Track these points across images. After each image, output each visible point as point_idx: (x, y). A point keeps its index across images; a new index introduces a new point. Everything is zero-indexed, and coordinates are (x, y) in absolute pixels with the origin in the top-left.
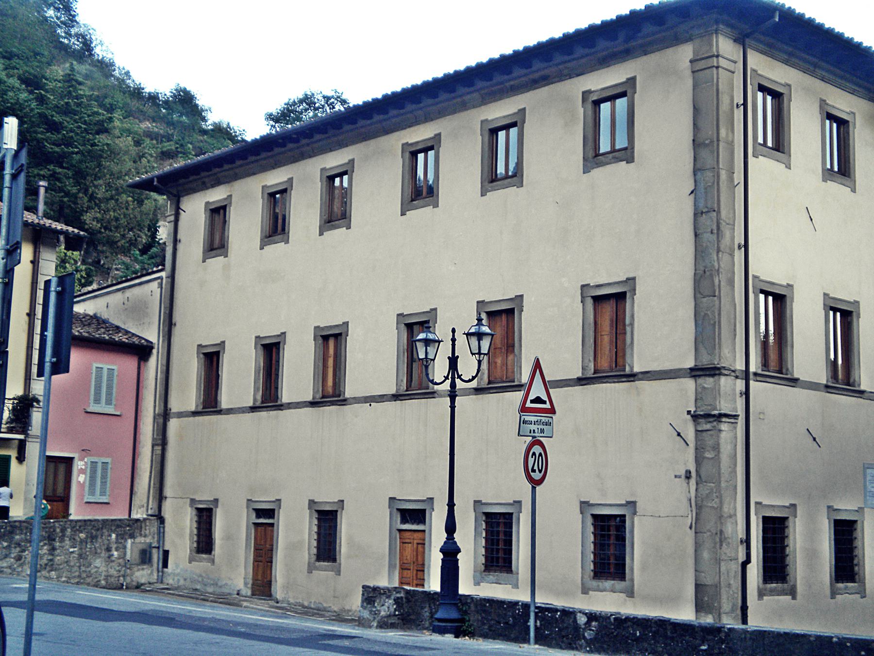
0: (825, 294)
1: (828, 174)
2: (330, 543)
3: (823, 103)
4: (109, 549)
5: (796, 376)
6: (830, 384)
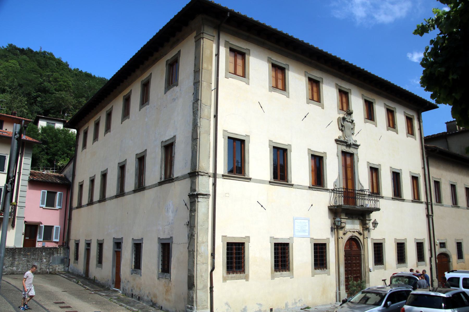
1: (275, 87)
2: (322, 252)
4: (41, 259)
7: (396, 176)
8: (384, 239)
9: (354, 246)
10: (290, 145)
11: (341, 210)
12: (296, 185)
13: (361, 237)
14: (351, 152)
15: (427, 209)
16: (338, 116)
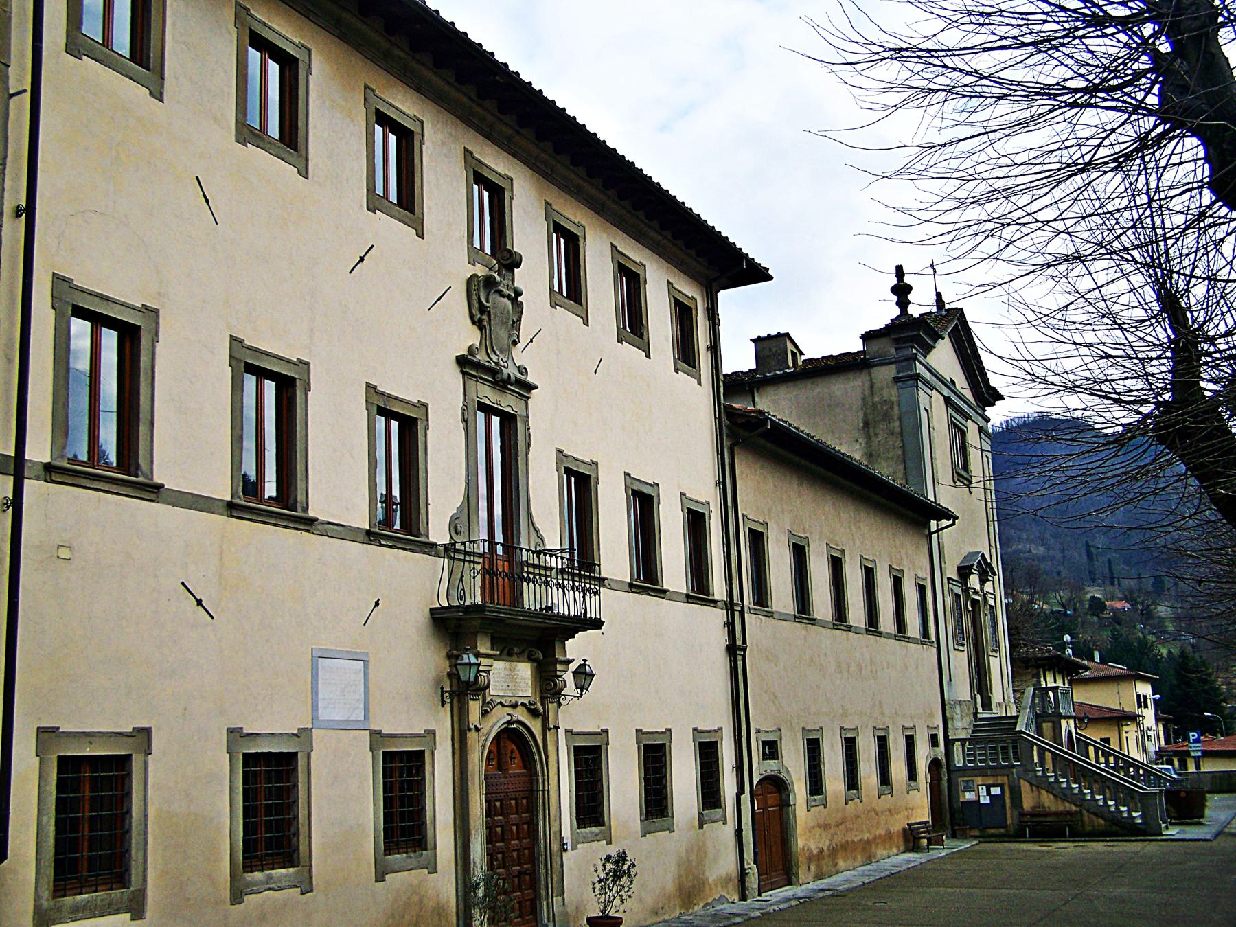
0: (369, 386)
3: (467, 152)
5: (157, 479)
6: (237, 501)
7: (644, 504)
8: (606, 731)
9: (517, 749)
10: (308, 364)
11: (477, 623)
12: (323, 523)
13: (536, 726)
14: (509, 410)
15: (730, 624)
16: (470, 270)
